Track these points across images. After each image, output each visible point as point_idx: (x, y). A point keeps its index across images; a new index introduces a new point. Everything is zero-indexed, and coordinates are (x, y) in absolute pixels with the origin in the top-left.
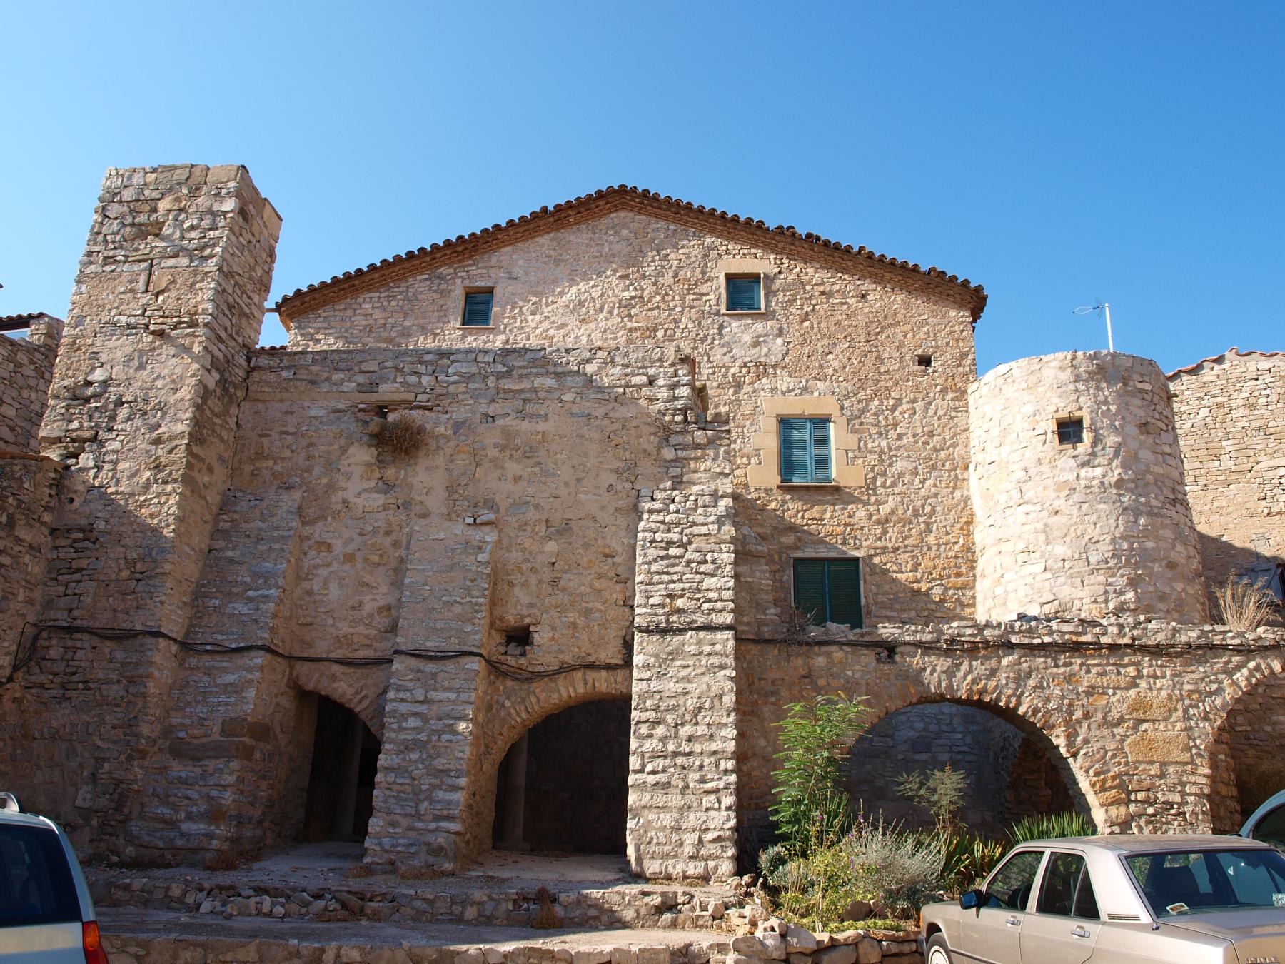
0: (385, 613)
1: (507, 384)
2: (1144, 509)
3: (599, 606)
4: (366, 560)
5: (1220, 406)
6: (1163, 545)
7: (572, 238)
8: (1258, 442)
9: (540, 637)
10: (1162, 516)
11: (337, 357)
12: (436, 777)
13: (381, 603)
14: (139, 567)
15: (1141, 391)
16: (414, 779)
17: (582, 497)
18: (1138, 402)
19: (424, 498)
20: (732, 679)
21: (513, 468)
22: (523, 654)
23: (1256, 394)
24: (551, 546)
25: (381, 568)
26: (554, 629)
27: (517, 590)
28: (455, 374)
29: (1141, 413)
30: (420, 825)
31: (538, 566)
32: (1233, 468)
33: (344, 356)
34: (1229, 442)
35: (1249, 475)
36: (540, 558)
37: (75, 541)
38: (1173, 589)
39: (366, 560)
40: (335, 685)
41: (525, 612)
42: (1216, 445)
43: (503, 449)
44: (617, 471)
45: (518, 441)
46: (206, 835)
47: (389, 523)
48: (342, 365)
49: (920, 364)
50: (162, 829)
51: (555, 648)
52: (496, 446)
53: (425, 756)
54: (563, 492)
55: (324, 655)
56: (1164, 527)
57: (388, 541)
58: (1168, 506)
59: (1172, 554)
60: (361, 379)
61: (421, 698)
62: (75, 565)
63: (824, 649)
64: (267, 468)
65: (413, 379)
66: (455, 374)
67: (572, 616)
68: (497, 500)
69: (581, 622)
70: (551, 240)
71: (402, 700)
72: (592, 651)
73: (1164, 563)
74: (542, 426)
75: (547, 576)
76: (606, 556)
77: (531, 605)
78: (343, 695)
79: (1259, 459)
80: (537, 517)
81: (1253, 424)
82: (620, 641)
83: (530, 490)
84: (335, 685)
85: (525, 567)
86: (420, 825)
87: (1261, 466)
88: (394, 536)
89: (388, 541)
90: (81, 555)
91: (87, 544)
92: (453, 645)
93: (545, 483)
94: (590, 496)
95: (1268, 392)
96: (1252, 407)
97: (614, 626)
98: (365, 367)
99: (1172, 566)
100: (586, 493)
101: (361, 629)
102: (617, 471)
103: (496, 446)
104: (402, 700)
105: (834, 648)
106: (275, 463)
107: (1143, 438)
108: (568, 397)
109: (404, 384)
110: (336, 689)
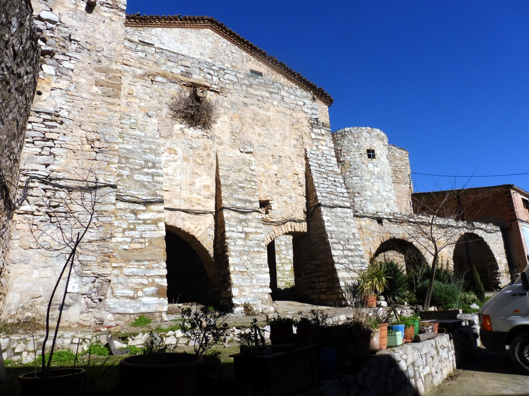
0: (207, 189)
1: (251, 90)
3: (294, 195)
4: (195, 161)
7: (188, 33)
9: (274, 205)
11: (169, 54)
12: (257, 268)
13: (204, 184)
14: (97, 144)
16: (247, 269)
17: (285, 148)
19: (220, 136)
21: (258, 130)
22: (267, 213)
24: (275, 167)
25: (202, 166)
26: (279, 203)
27: (263, 184)
28: (228, 79)
30: (254, 290)
31: (271, 175)
33: (172, 54)
36: (271, 171)
37: (45, 120)
39: (195, 161)
40: (185, 223)
41: (267, 195)
43: (253, 120)
44: (296, 139)
45: (258, 118)
46: (159, 304)
47: (206, 145)
48: (172, 59)
50: (129, 303)
51: (280, 211)
52: (250, 118)
53: (249, 258)
54: (278, 144)
55: (178, 208)
57: (205, 154)
60: (183, 69)
61: (241, 231)
62: (48, 136)
63: (364, 219)
64: (135, 103)
65: (209, 76)
66: (228, 79)
67: (285, 198)
68: (253, 142)
69: (289, 201)
70: (179, 31)
71: (232, 231)
72: (293, 214)
74: (268, 114)
75: (275, 180)
76: (295, 174)
77: (269, 192)
78: (189, 228)
80: (269, 153)
83: (266, 141)
84: (185, 223)
85: (266, 174)
86: (254, 290)
88: (208, 151)
89: (205, 154)
90: (51, 130)
91: (54, 124)
92: (201, 208)
93: (271, 139)
94: (288, 148)
97: (300, 204)
98: (184, 63)
100: (287, 146)
101: (195, 195)
102: (296, 139)
103: (250, 118)
104: (232, 231)
105: (367, 218)
106: (141, 101)
108: (275, 103)
109: (204, 77)
110: (184, 225)
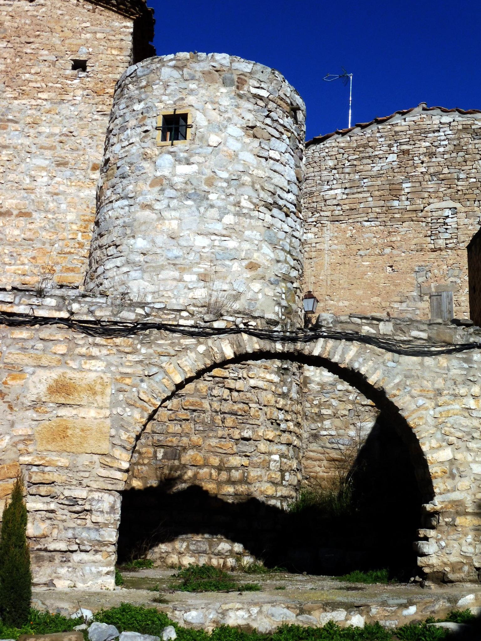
2: (232, 208)
5: (404, 152)
6: (246, 246)
8: (431, 186)
10: (251, 217)
15: (256, 96)
18: (250, 106)
20: (423, 555)
23: (436, 144)
29: (249, 116)
32: (408, 208)
34: (409, 185)
35: (420, 214)
38: (249, 289)
42: (397, 187)
49: (74, 68)
56: (252, 228)
58: (262, 209)
59: (256, 255)
73: (245, 263)
79: (431, 201)
81: (432, 170)
82: (53, 480)
87: (432, 206)
95: (446, 142)
96: (432, 155)
99: (252, 266)
107: (247, 140)
